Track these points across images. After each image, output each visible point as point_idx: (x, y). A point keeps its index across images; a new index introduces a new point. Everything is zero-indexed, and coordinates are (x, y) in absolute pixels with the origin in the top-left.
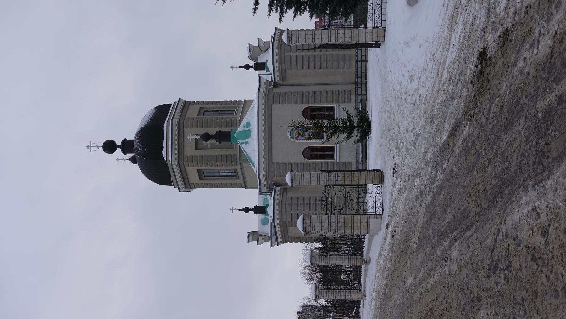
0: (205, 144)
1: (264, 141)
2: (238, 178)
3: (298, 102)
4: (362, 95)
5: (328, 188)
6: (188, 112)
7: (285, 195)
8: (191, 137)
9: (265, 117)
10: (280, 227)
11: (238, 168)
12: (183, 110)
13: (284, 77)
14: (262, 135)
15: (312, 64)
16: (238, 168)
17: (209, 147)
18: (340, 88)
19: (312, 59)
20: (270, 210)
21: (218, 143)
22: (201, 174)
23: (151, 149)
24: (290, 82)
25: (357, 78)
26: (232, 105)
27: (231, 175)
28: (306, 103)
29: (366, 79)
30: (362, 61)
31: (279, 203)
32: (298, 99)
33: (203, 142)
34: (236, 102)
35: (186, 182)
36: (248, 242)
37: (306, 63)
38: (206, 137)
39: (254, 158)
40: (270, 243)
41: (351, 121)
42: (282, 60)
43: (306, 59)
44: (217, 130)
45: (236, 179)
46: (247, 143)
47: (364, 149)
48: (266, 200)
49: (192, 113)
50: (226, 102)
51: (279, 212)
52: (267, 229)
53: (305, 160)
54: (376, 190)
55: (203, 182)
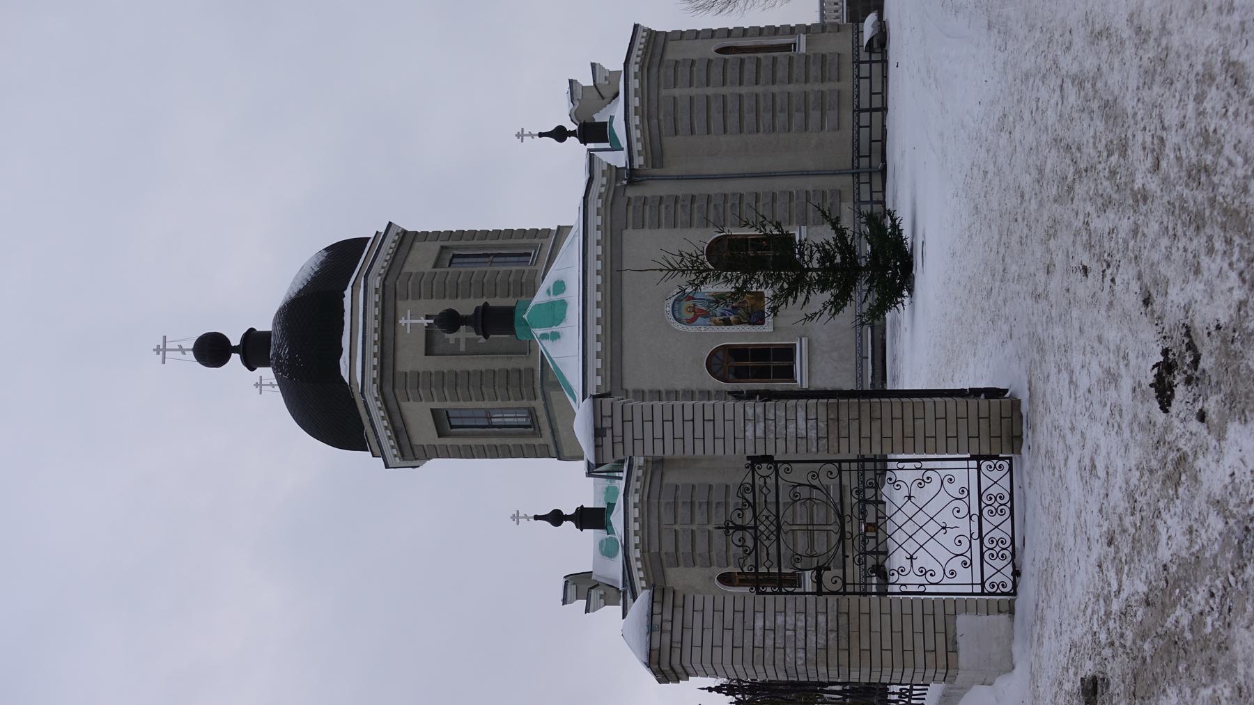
0: (452, 342)
1: (599, 330)
2: (538, 433)
3: (695, 222)
4: (871, 202)
5: (764, 469)
6: (409, 259)
8: (409, 321)
9: (604, 265)
10: (645, 568)
11: (538, 404)
12: (396, 253)
13: (656, 155)
14: (595, 313)
15: (733, 119)
16: (538, 404)
17: (462, 348)
18: (810, 184)
19: (732, 105)
20: (617, 519)
21: (482, 340)
22: (442, 422)
23: (320, 356)
24: (673, 170)
25: (859, 157)
26: (525, 241)
27: (511, 421)
29: (884, 159)
30: (871, 110)
31: (641, 500)
32: (696, 216)
33: (447, 335)
34: (535, 233)
35: (404, 441)
36: (565, 601)
37: (717, 116)
38: (450, 321)
39: (574, 377)
40: (620, 608)
41: (848, 250)
42: (648, 113)
43: (716, 106)
44: (480, 302)
45: (534, 435)
46: (556, 336)
47: (879, 350)
48: (611, 492)
49: (421, 261)
50: (510, 233)
51: (642, 526)
52: (614, 570)
53: (713, 383)
55: (448, 441)
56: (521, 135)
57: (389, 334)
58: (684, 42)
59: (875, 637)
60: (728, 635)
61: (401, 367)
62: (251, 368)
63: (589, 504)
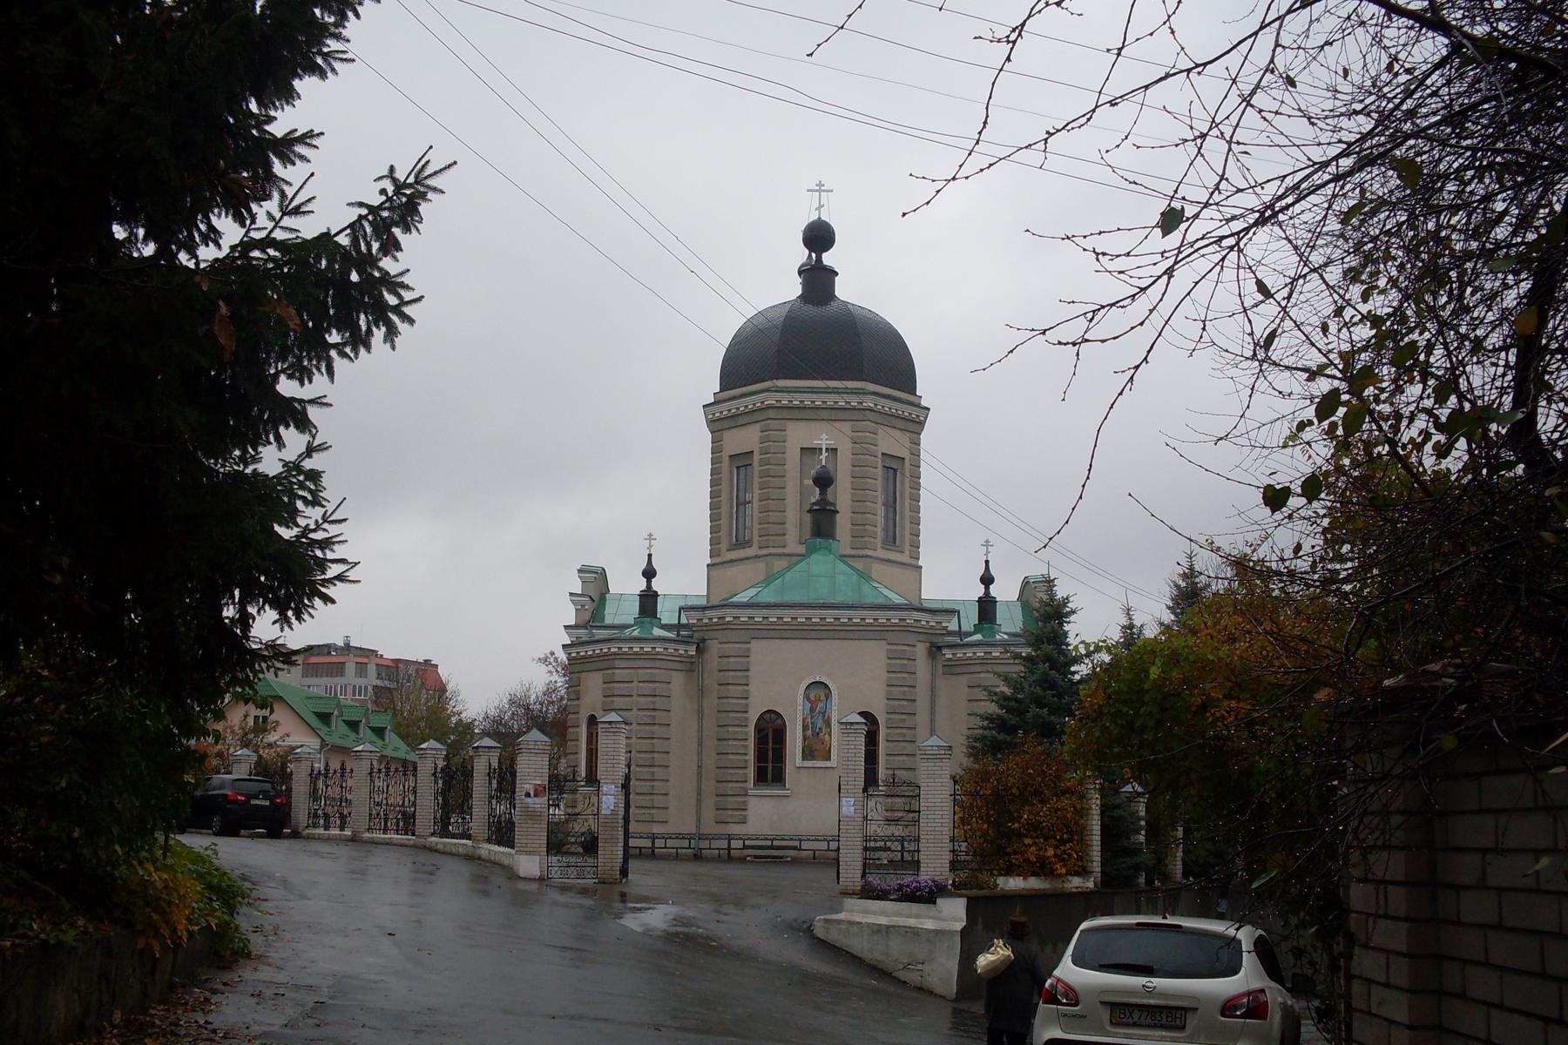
7: (678, 666)
22: (742, 461)
28: (888, 720)
38: (824, 481)
49: (890, 441)
51: (636, 654)
53: (753, 716)
55: (726, 463)
56: (987, 544)
61: (791, 426)
62: (800, 273)
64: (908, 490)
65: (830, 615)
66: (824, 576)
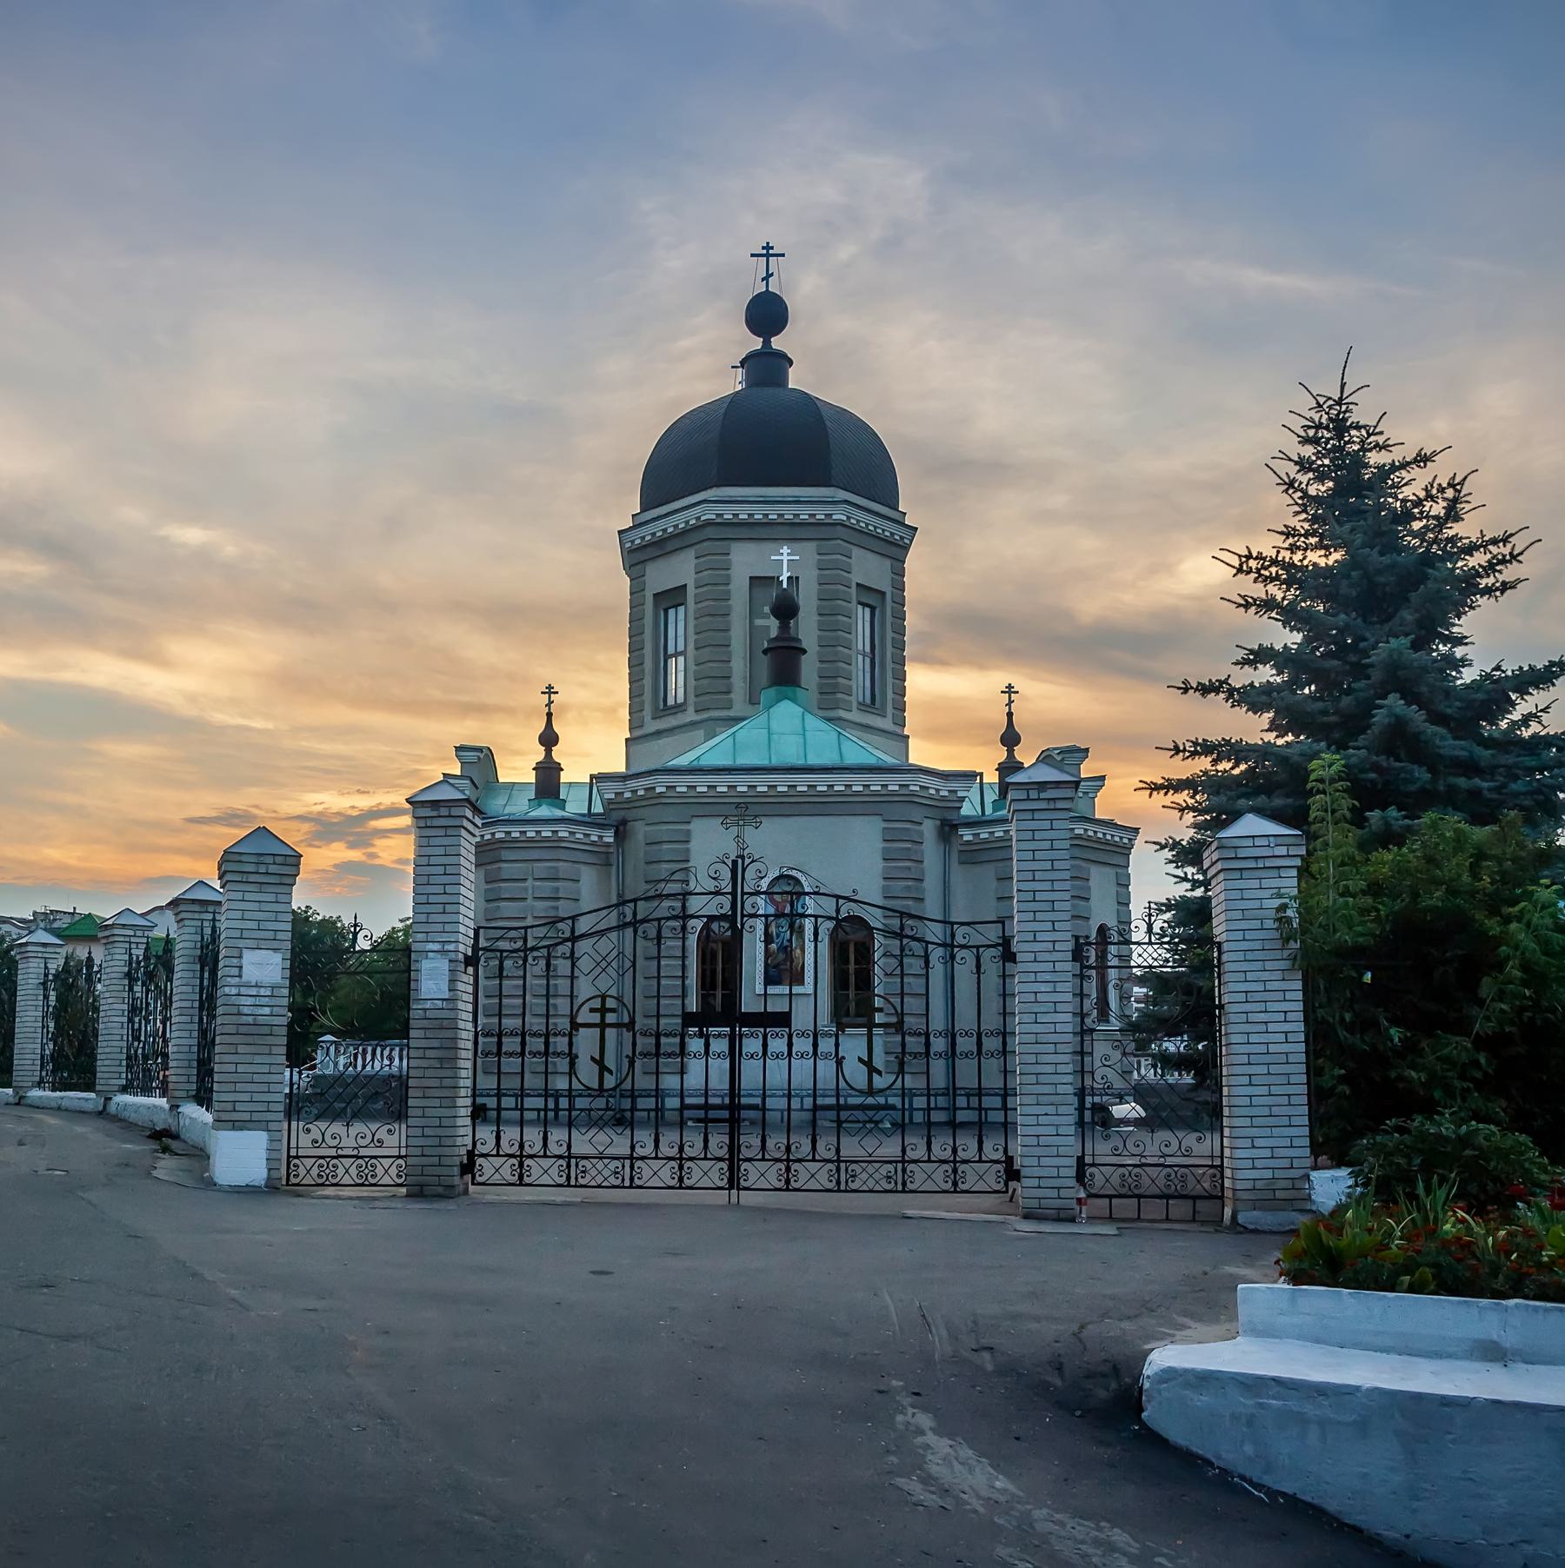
6: (870, 555)
8: (785, 558)
11: (690, 716)
16: (690, 716)
17: (759, 622)
22: (672, 598)
31: (562, 840)
35: (651, 552)
38: (786, 610)
49: (867, 568)
51: (531, 840)
54: (386, 1162)
57: (763, 533)
58: (1114, 889)
59: (248, 1059)
60: (253, 925)
63: (564, 777)
64: (890, 635)
65: (802, 782)
66: (787, 733)
